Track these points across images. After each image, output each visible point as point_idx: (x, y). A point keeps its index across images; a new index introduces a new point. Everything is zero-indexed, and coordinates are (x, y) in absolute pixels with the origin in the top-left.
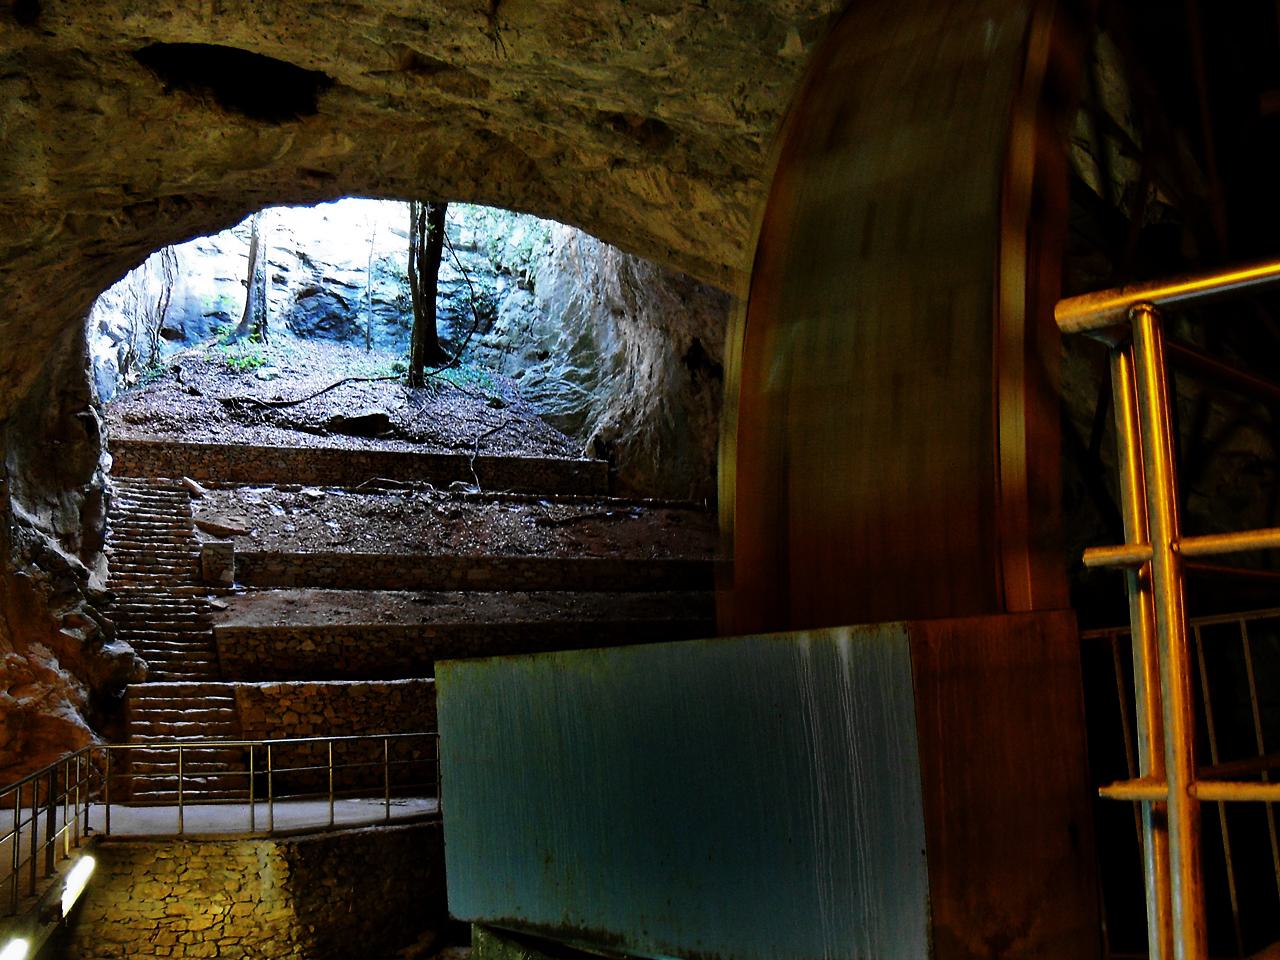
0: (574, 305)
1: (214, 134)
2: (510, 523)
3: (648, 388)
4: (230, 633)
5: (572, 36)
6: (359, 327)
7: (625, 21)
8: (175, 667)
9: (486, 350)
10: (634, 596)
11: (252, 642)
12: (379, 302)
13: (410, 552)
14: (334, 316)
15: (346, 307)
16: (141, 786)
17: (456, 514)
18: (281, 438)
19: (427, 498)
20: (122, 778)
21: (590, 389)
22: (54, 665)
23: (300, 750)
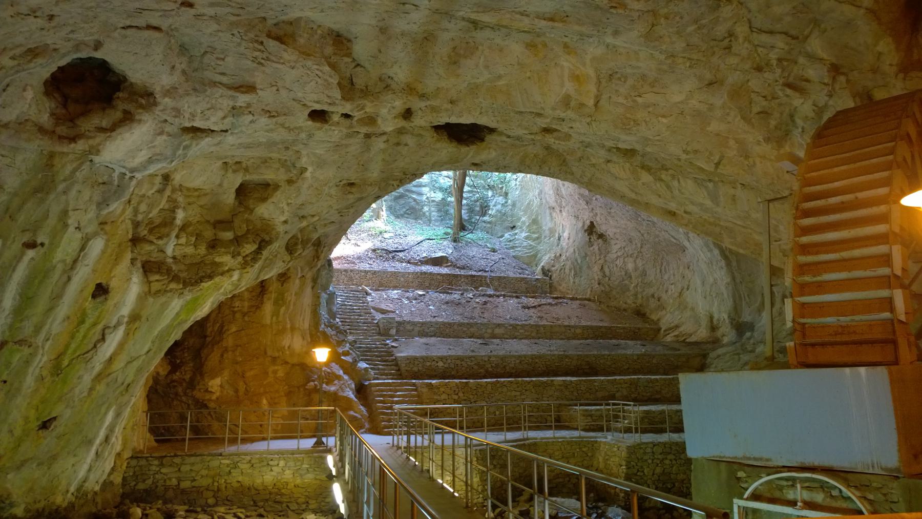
0: (529, 204)
1: (445, 151)
2: (509, 309)
3: (568, 244)
5: (624, 124)
6: (424, 213)
7: (648, 119)
8: (383, 374)
9: (484, 225)
11: (416, 362)
12: (433, 201)
13: (466, 321)
14: (412, 208)
15: (418, 203)
16: (386, 427)
17: (485, 303)
18: (400, 267)
19: (470, 295)
21: (539, 244)
22: (341, 372)
23: (449, 411)
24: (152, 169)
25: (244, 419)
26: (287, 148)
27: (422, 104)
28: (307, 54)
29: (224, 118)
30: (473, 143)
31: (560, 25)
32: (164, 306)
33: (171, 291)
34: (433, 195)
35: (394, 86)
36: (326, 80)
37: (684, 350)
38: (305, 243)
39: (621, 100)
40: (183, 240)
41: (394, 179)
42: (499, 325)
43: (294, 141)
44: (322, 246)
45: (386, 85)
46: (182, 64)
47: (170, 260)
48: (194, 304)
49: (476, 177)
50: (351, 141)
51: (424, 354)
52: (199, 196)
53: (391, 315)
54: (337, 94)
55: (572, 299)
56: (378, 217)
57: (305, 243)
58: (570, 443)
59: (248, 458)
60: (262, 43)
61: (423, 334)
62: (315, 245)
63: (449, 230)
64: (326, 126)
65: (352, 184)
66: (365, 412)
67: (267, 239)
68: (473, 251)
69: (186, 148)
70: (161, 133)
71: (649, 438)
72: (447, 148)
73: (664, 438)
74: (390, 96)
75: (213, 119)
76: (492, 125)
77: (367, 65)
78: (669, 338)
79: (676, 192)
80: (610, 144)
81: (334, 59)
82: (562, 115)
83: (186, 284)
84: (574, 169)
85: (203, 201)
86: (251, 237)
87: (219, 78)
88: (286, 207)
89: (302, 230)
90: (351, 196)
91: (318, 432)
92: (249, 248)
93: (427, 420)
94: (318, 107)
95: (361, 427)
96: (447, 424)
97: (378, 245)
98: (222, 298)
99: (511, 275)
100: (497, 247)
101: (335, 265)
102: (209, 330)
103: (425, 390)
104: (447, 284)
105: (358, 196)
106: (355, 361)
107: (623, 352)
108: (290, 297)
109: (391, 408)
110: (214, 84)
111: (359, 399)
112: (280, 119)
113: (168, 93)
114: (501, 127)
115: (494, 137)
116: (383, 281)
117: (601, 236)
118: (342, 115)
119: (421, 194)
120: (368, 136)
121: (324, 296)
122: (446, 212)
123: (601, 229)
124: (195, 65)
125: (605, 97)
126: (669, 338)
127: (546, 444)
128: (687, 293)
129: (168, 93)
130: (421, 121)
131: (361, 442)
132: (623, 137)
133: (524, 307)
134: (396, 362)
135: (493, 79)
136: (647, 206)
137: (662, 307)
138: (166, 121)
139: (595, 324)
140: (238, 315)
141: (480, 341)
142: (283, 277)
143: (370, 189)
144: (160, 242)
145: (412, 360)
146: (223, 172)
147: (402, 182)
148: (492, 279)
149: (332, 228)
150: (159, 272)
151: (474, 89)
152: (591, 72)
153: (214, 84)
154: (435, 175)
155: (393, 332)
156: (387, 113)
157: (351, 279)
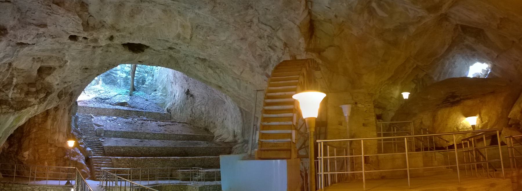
1: (127, 55)
2: (152, 126)
4: (108, 147)
10: (180, 141)
14: (113, 80)
17: (142, 123)
18: (107, 106)
20: (500, 167)
22: (79, 152)
24: (5, 61)
25: (38, 170)
26: (59, 52)
27: (118, 34)
28: (69, 11)
29: (34, 38)
30: (139, 52)
31: (177, 3)
32: (7, 119)
33: (10, 112)
34: (122, 74)
35: (106, 25)
36: (77, 22)
37: (224, 146)
38: (66, 94)
39: (201, 37)
40: (15, 91)
41: (105, 67)
42: (148, 133)
43: (63, 49)
44: (73, 95)
45: (102, 25)
46: (18, 16)
47: (10, 100)
48: (18, 119)
49: (140, 67)
50: (87, 49)
51: (115, 145)
52: (22, 72)
53: (102, 127)
54: (81, 28)
55: (179, 123)
56: (98, 83)
57: (66, 94)
58: (176, 186)
59: (38, 187)
60: (50, 6)
61: (115, 136)
62: (70, 95)
63: (128, 91)
64: (76, 43)
65: (87, 69)
66: (89, 170)
67: (50, 91)
68: (138, 100)
69: (18, 51)
70: (9, 46)
71: (208, 183)
72: (128, 54)
73: (214, 183)
74: (104, 30)
75: (29, 39)
76: (147, 45)
77: (94, 16)
78: (218, 140)
79: (222, 78)
80: (196, 56)
81: (80, 13)
82: (177, 42)
83: (16, 110)
84: (181, 66)
85: (24, 74)
86: (43, 91)
87: (32, 21)
88: (58, 78)
89: (65, 88)
90: (86, 74)
91: (68, 178)
92: (42, 95)
93: (115, 175)
94: (73, 34)
95: (87, 177)
96: (124, 177)
97: (98, 96)
98: (30, 117)
99: (154, 111)
100: (148, 99)
101: (79, 104)
102: (25, 130)
103: (115, 161)
104: (126, 114)
105: (89, 74)
106: (85, 147)
107: (199, 146)
108: (59, 118)
109: (100, 169)
110: (30, 24)
111: (86, 164)
112: (57, 39)
113: (12, 28)
114: (151, 46)
115: (148, 50)
116: (99, 112)
117: (192, 96)
118: (83, 38)
119: (117, 74)
120: (94, 47)
121: (73, 118)
122: (127, 82)
123: (192, 92)
124: (23, 16)
125: (194, 35)
126: (218, 140)
127: (166, 186)
128: (225, 121)
129: (12, 28)
130: (117, 41)
131: (85, 183)
132: (201, 53)
133: (159, 126)
134: (103, 149)
135: (149, 24)
136: (210, 83)
137: (215, 127)
138: (11, 40)
139: (188, 134)
140: (36, 125)
141: (139, 140)
142: (56, 109)
143: (94, 71)
144: (7, 92)
145: (110, 148)
146: (32, 62)
147: (108, 68)
148: (146, 113)
149: (78, 87)
150: (6, 104)
151: (140, 28)
152: (189, 24)
153: (30, 24)
154: (123, 66)
155: (102, 135)
156: (103, 37)
157: (85, 111)
